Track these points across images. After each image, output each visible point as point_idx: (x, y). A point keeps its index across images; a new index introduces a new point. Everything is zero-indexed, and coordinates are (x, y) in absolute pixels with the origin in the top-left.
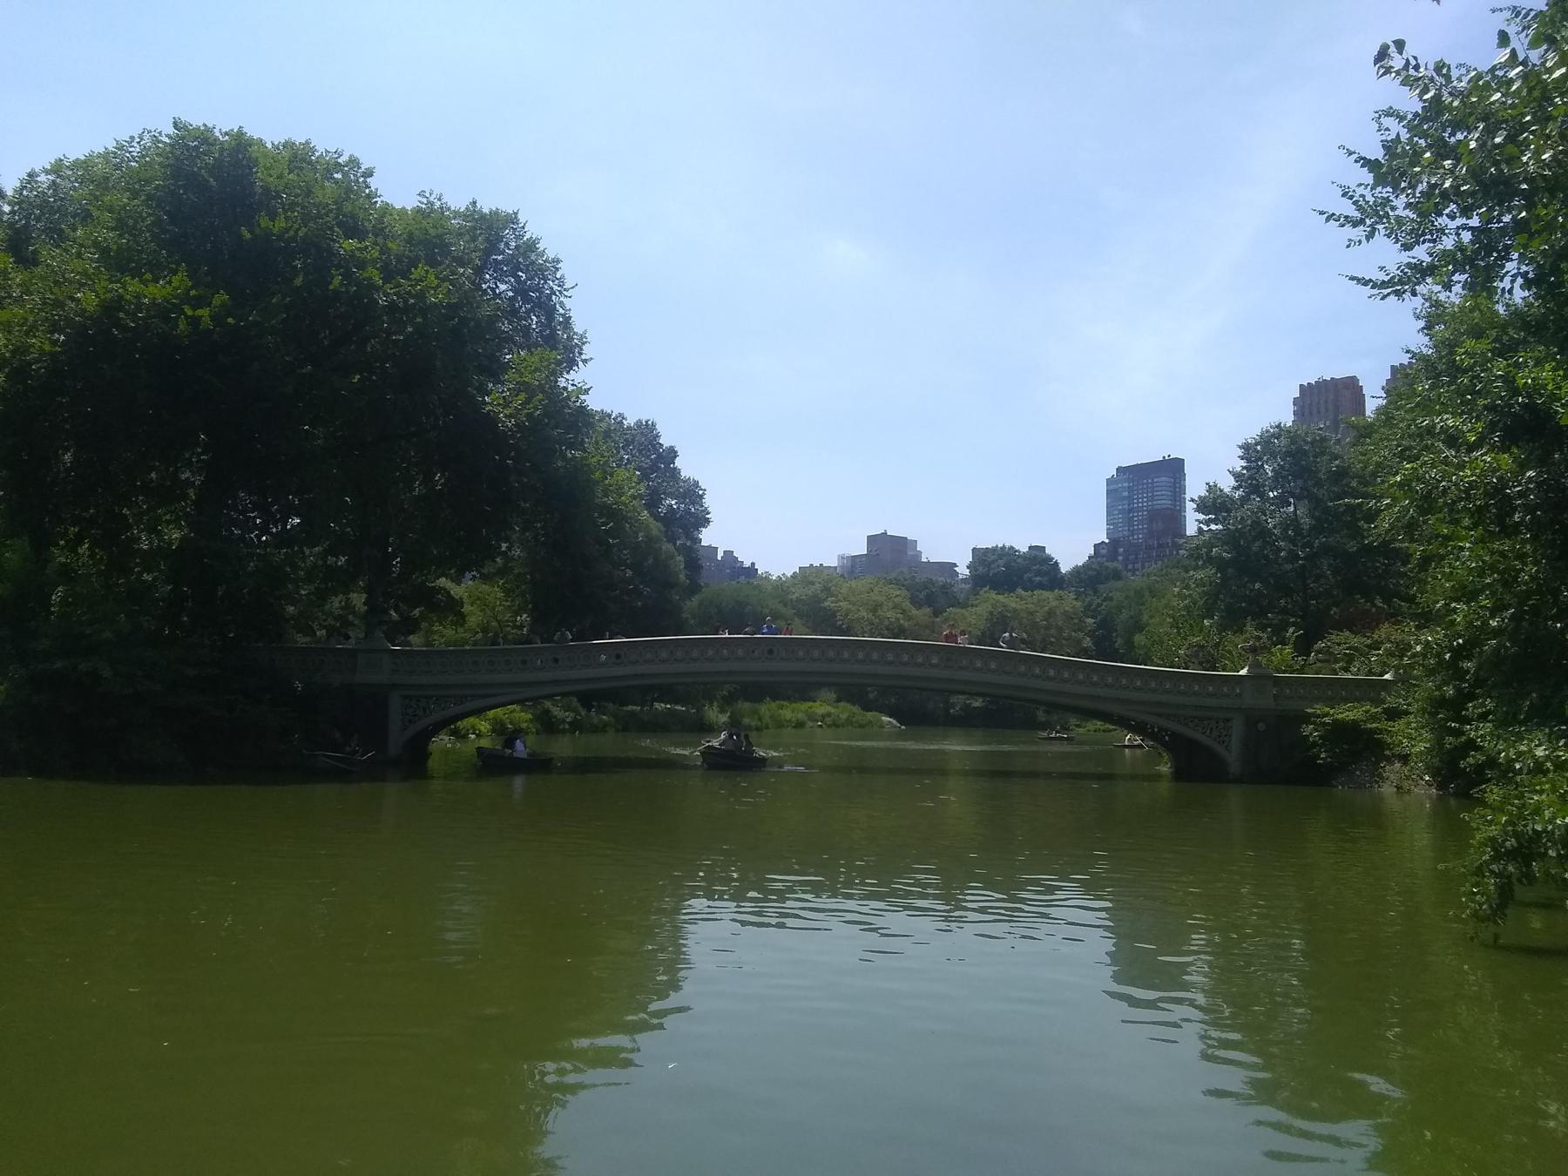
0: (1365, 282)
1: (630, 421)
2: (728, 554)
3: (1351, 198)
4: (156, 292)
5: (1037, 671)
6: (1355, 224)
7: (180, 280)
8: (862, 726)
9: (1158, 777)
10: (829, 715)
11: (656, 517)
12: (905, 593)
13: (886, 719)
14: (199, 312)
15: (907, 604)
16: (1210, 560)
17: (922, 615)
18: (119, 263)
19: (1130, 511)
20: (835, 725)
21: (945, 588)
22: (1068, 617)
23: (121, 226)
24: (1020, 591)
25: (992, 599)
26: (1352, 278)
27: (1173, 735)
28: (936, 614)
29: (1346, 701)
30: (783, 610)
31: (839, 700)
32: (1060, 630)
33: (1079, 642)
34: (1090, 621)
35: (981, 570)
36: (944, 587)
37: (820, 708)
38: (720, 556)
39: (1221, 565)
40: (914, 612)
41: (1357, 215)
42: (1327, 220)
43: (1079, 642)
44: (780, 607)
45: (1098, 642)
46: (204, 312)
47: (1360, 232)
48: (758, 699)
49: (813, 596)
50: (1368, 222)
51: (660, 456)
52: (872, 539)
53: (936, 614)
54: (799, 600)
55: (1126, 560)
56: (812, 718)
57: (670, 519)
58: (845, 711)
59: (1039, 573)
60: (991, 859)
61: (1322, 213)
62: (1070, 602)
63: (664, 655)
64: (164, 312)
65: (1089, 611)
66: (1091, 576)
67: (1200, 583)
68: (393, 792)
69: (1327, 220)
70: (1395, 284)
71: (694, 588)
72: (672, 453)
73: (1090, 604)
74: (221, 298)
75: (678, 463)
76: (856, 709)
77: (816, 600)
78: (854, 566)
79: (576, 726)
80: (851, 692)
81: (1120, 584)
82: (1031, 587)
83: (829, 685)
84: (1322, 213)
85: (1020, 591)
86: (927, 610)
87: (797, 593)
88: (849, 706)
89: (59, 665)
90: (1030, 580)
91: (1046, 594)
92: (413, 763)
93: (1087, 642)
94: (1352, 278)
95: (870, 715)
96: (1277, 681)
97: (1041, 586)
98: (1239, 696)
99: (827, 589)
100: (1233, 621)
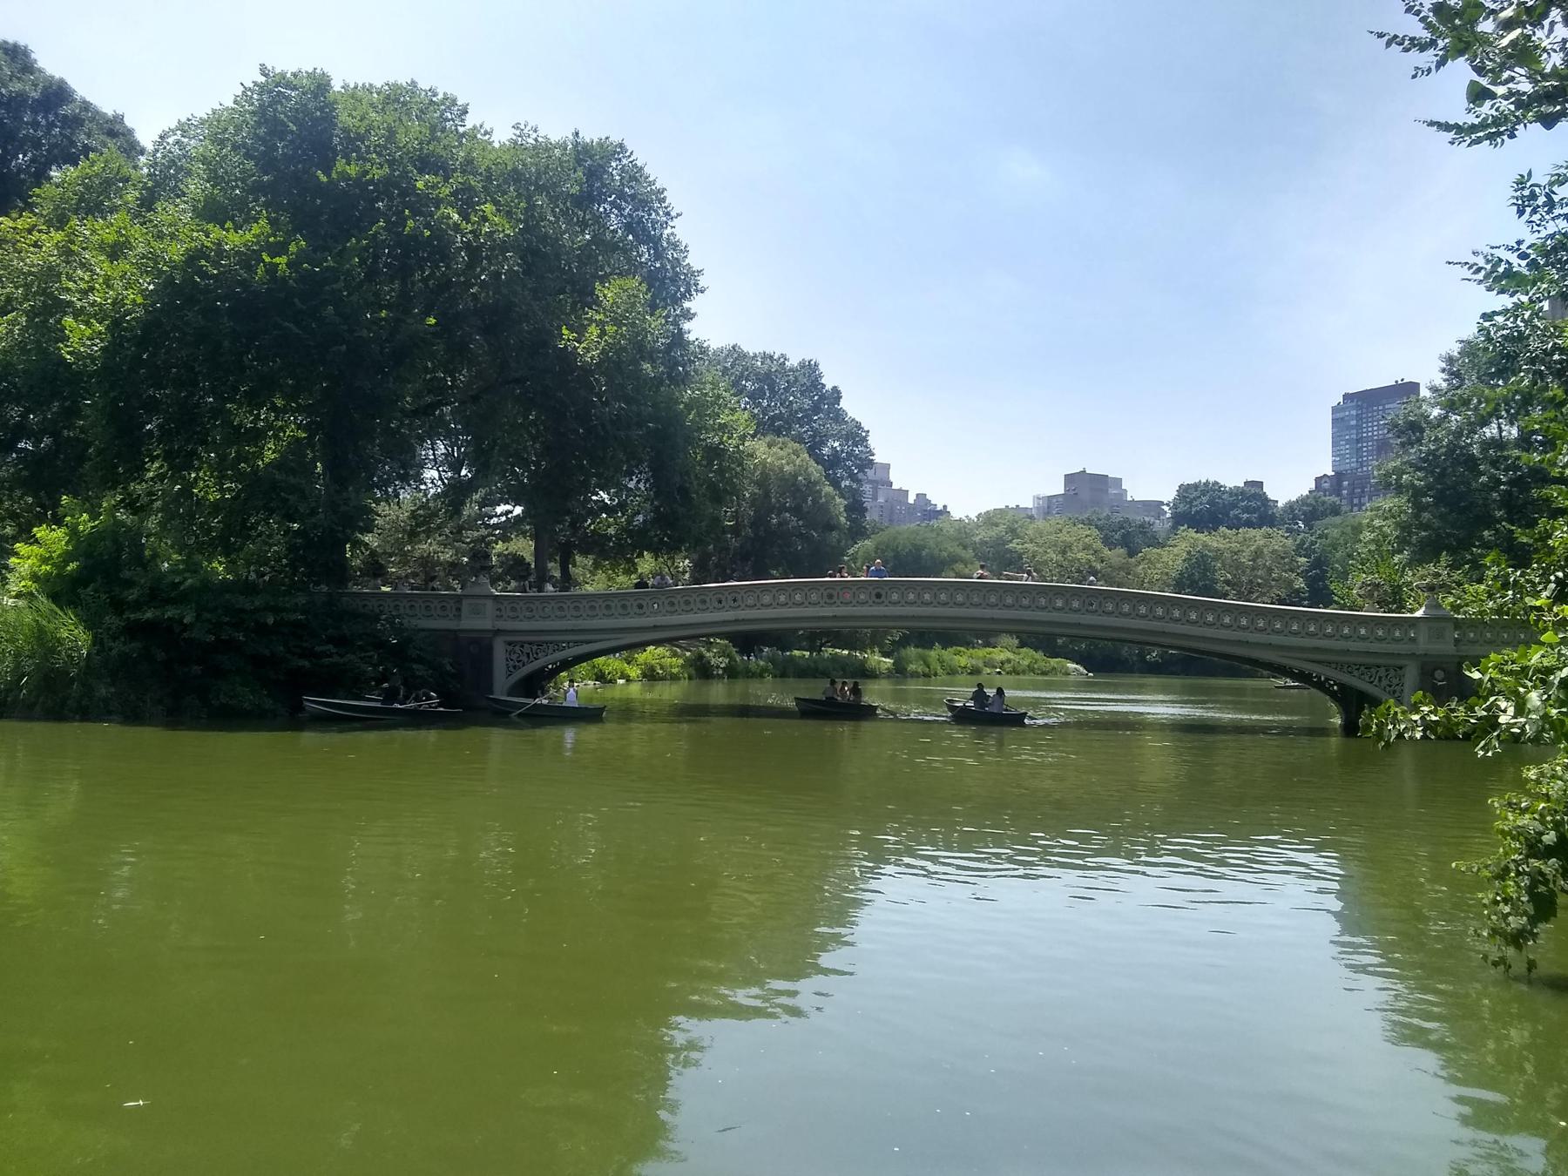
0: (1446, 127)
1: (793, 362)
2: (921, 497)
3: (1418, 13)
4: (234, 240)
5: (1210, 619)
6: (1423, 47)
7: (260, 227)
8: (1044, 673)
9: (1323, 732)
10: (1009, 661)
11: (819, 460)
12: (1095, 532)
13: (1072, 666)
14: (277, 260)
15: (1098, 545)
16: (1399, 489)
17: (1117, 555)
18: (212, 212)
19: (1358, 441)
20: (1015, 672)
21: (1143, 528)
22: (1279, 557)
23: (214, 178)
24: (1222, 529)
25: (1190, 540)
26: (1431, 124)
27: (1342, 686)
28: (1131, 554)
29: (1506, 644)
30: (963, 553)
31: (1022, 645)
32: (1270, 570)
33: (1290, 583)
34: (1303, 560)
35: (1182, 508)
36: (1142, 526)
37: (999, 655)
38: (911, 500)
39: (1417, 494)
40: (1106, 552)
41: (1425, 35)
42: (1388, 44)
43: (1290, 583)
44: (959, 551)
45: (1311, 582)
46: (282, 260)
47: (1429, 58)
48: (929, 645)
49: (999, 543)
50: (1441, 44)
51: (822, 397)
52: (1069, 478)
53: (1131, 554)
54: (983, 543)
55: (1352, 494)
56: (989, 664)
57: (832, 462)
58: (1027, 656)
59: (1247, 510)
60: (1211, 804)
61: (1381, 35)
62: (1280, 540)
63: (767, 599)
64: (248, 259)
65: (1300, 549)
66: (1310, 510)
67: (1389, 515)
68: (498, 739)
69: (1388, 44)
70: (1488, 126)
71: (858, 531)
72: (836, 394)
73: (1303, 542)
74: (298, 245)
75: (843, 404)
76: (1039, 655)
77: (1000, 542)
78: (1050, 505)
79: (732, 672)
80: (1044, 641)
81: (1338, 519)
82: (1235, 525)
83: (1010, 633)
84: (1381, 35)
85: (1222, 529)
86: (1122, 551)
87: (981, 535)
88: (1032, 652)
89: (149, 615)
90: (1236, 517)
91: (1252, 532)
92: (529, 706)
93: (1300, 583)
94: (1431, 124)
95: (1054, 662)
96: (1457, 624)
97: (1249, 524)
98: (1413, 640)
99: (1013, 531)
100: (1426, 552)
